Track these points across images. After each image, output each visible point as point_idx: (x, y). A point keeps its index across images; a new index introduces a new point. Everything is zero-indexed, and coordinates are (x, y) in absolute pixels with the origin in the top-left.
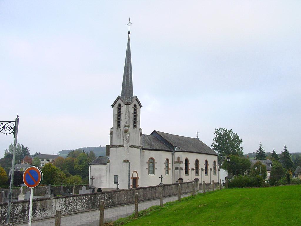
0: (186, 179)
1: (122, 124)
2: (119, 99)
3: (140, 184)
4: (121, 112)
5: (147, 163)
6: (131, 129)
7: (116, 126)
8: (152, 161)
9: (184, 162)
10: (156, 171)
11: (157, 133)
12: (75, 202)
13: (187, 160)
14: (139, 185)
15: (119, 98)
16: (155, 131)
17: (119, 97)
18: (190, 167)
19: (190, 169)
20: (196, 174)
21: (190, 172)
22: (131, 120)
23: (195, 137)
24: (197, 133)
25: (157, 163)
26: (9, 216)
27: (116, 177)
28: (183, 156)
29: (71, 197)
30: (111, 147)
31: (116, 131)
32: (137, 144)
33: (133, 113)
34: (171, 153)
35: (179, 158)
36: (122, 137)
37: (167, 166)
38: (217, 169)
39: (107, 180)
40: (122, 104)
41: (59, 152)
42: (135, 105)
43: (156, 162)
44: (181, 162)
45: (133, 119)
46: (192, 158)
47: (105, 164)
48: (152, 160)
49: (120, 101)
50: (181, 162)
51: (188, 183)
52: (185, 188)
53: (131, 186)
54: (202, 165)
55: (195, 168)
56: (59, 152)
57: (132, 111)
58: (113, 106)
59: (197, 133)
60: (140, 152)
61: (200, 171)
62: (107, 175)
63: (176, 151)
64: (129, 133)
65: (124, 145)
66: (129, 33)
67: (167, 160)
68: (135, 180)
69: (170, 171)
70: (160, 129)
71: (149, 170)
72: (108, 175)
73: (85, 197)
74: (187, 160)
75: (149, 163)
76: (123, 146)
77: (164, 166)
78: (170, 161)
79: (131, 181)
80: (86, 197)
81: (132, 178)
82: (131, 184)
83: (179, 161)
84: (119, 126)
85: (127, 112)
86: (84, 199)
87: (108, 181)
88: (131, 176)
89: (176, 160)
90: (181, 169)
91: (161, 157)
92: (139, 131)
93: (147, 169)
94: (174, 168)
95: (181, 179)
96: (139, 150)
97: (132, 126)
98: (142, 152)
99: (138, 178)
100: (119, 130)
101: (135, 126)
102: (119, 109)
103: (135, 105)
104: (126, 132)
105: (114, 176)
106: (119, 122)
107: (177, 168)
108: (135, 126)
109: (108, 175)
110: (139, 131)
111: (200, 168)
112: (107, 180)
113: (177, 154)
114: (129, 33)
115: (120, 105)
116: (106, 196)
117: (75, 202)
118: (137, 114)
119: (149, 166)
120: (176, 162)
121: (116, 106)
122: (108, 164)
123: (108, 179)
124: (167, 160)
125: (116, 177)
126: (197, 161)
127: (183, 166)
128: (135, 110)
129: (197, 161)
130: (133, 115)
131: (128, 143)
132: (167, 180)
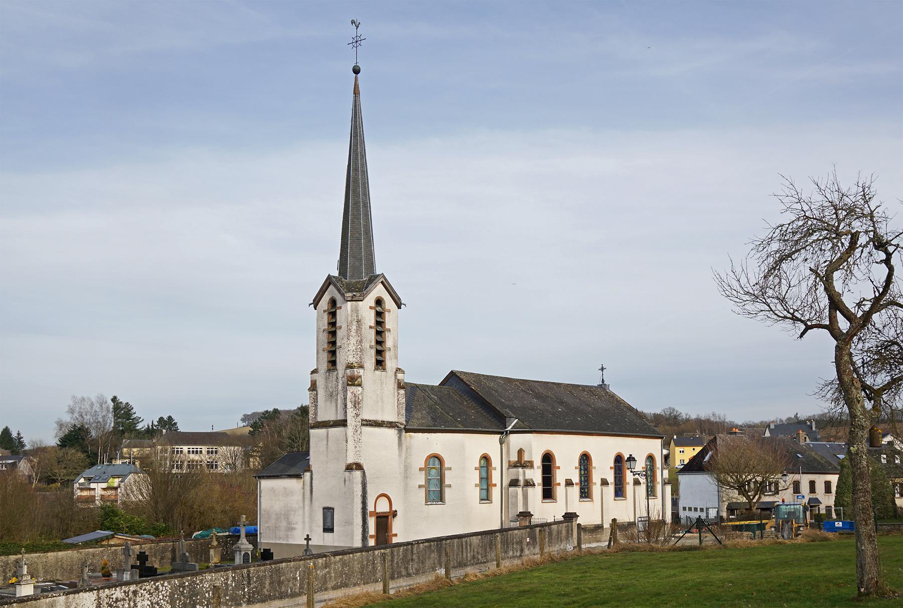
0: (546, 512)
1: (342, 359)
2: (330, 284)
3: (401, 532)
4: (338, 325)
5: (421, 469)
6: (368, 374)
7: (324, 366)
8: (437, 465)
9: (538, 462)
10: (447, 491)
11: (462, 380)
12: (130, 600)
13: (548, 459)
14: (396, 535)
15: (329, 281)
16: (452, 374)
17: (329, 277)
18: (560, 477)
19: (559, 484)
20: (581, 497)
21: (560, 491)
22: (366, 345)
23: (596, 382)
24: (602, 369)
25: (450, 469)
26: (490, 548)
27: (328, 512)
28: (535, 445)
29: (117, 586)
30: (312, 428)
31: (327, 379)
32: (391, 417)
33: (373, 323)
34: (497, 437)
35: (520, 452)
36: (340, 397)
37: (484, 475)
38: (659, 479)
39: (304, 522)
40: (338, 298)
41: (243, 420)
42: (379, 302)
43: (450, 466)
44: (530, 465)
45: (373, 343)
46: (567, 448)
47: (298, 476)
48: (437, 461)
49: (332, 291)
50: (530, 465)
51: (542, 526)
52: (520, 543)
53: (371, 537)
54: (603, 469)
55: (576, 479)
56: (243, 420)
57: (369, 318)
58: (316, 303)
59: (602, 369)
60: (400, 438)
61: (596, 489)
62: (304, 508)
63: (512, 432)
64: (360, 385)
65: (346, 421)
66: (356, 71)
67: (486, 458)
68: (384, 521)
69: (496, 493)
70: (458, 368)
71: (428, 493)
72: (307, 508)
73: (163, 586)
74: (548, 459)
75: (426, 469)
76: (343, 423)
77: (475, 477)
78: (496, 462)
79: (372, 522)
80: (166, 584)
81: (372, 514)
82: (372, 530)
83: (522, 463)
84: (333, 363)
85: (355, 323)
86: (157, 589)
87: (307, 525)
88: (370, 508)
89: (514, 458)
90: (529, 484)
91: (464, 450)
92: (396, 376)
93: (420, 487)
94: (506, 482)
95: (526, 515)
96: (392, 433)
97: (370, 360)
98: (403, 438)
99: (395, 514)
100: (335, 378)
101: (380, 364)
102: (333, 314)
103: (379, 302)
104: (353, 381)
105: (324, 508)
106: (333, 353)
107: (514, 483)
108: (380, 364)
109: (307, 508)
110: (396, 376)
111: (596, 478)
112: (304, 522)
113: (517, 441)
114: (356, 71)
115: (333, 302)
116: (231, 579)
117: (130, 600)
118: (387, 327)
119: (428, 481)
120: (515, 465)
121: (324, 303)
122: (308, 474)
123: (307, 520)
124: (486, 458)
125: (328, 512)
126: (585, 459)
127: (536, 475)
128: (379, 314)
129: (585, 459)
130: (373, 332)
131: (357, 415)
132: (489, 517)
